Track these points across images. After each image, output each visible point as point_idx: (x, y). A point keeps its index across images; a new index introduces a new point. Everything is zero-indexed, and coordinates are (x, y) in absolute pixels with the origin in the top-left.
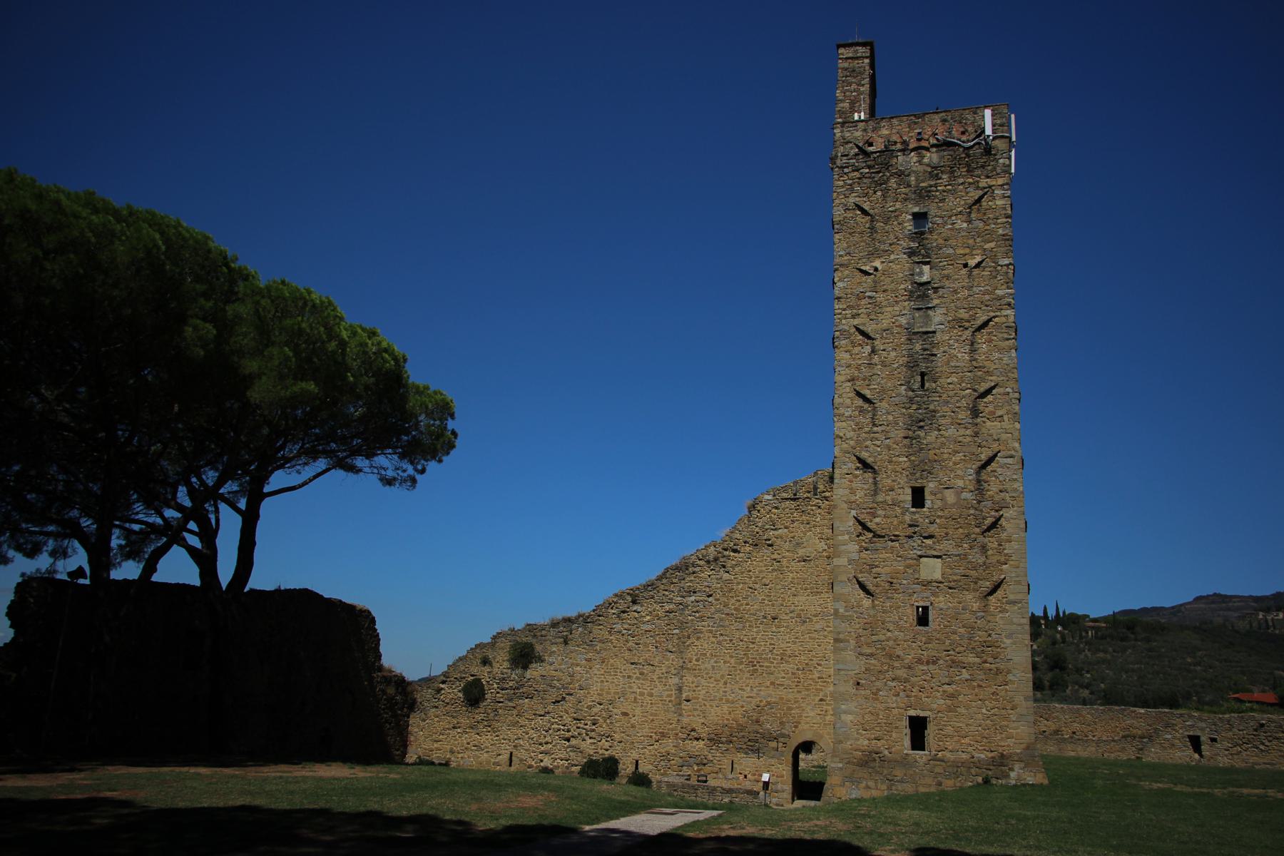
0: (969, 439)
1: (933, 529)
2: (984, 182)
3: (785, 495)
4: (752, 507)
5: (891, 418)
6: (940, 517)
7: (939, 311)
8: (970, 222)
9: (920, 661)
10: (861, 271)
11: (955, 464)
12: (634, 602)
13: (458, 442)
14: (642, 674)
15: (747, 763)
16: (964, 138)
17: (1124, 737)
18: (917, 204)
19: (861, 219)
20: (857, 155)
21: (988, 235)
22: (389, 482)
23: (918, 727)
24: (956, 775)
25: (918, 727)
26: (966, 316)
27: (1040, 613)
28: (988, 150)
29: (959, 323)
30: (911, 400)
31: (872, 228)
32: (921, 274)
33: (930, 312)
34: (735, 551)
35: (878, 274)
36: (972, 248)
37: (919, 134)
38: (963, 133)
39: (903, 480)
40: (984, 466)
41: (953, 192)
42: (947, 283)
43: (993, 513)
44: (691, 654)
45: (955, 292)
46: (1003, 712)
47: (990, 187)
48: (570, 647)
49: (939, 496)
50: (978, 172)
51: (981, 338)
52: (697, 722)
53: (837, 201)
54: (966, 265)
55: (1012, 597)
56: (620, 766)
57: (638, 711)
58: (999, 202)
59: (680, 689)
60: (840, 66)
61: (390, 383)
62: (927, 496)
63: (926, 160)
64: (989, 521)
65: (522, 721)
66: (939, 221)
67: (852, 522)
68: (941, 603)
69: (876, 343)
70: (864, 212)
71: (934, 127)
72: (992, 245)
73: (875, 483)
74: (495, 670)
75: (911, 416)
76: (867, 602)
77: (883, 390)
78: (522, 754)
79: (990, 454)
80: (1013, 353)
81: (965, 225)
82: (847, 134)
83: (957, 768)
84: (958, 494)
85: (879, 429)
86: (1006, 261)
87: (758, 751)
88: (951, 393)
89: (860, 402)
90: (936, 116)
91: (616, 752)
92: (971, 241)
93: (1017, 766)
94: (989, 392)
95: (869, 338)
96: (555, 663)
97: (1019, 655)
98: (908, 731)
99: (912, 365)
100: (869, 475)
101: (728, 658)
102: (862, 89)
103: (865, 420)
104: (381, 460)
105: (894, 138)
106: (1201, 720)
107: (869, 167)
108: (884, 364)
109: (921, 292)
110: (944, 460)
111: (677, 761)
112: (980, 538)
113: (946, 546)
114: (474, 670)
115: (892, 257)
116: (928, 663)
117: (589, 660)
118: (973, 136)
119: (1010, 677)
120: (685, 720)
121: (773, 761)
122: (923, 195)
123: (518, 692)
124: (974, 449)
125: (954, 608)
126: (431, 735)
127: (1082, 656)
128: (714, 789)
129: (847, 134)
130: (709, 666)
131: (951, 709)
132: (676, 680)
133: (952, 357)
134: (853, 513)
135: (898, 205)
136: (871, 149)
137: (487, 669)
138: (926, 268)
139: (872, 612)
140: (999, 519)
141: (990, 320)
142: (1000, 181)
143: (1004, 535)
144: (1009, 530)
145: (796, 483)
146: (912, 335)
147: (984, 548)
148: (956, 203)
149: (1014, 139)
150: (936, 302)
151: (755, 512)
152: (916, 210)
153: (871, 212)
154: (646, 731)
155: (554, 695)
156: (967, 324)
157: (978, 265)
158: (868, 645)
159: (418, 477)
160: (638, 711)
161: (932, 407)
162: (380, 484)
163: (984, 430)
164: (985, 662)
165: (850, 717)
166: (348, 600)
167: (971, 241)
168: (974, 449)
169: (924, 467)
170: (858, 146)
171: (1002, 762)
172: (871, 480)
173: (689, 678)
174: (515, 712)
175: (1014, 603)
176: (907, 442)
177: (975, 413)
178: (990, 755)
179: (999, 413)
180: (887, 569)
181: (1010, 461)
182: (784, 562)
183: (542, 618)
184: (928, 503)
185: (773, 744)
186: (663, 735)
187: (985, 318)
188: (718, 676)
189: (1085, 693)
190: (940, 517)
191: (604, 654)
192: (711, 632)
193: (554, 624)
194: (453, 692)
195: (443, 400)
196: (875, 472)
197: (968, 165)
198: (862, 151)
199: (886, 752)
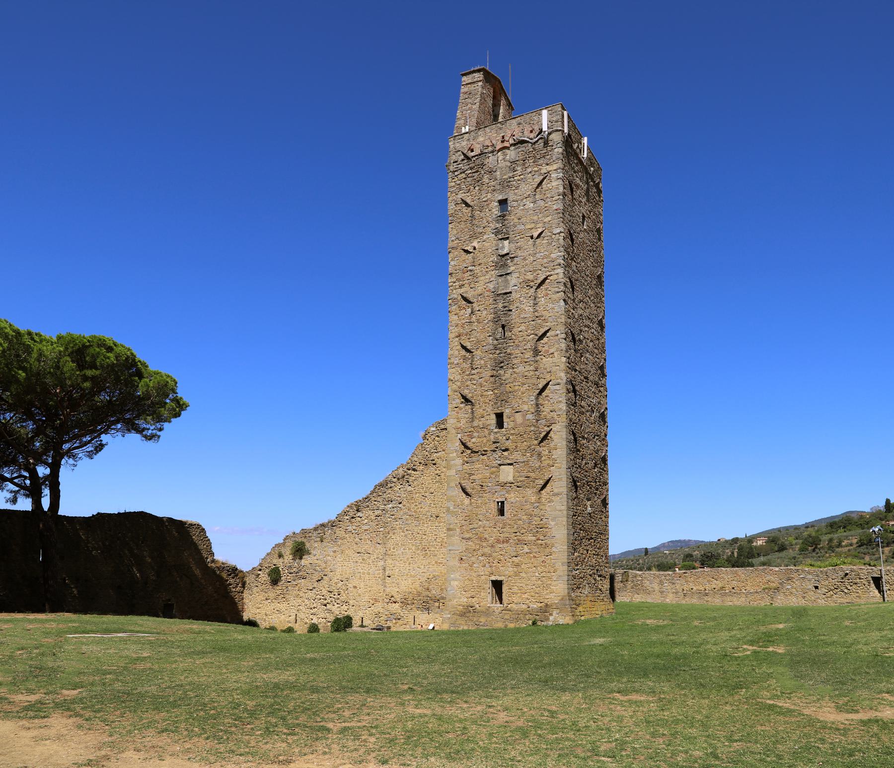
0: (532, 373)
1: (508, 444)
4: (424, 438)
5: (482, 362)
6: (512, 434)
7: (515, 275)
8: (534, 202)
9: (498, 541)
12: (358, 511)
16: (532, 135)
17: (764, 589)
18: (501, 192)
20: (463, 160)
23: (497, 586)
25: (497, 586)
29: (527, 284)
30: (496, 348)
32: (503, 247)
33: (509, 277)
34: (414, 470)
38: (531, 132)
39: (489, 409)
40: (540, 393)
42: (519, 253)
44: (390, 544)
45: (525, 259)
48: (324, 544)
49: (512, 419)
50: (541, 161)
52: (393, 590)
54: (532, 237)
55: (556, 491)
56: (353, 622)
58: (554, 184)
59: (384, 569)
61: (130, 368)
62: (505, 419)
65: (301, 594)
66: (515, 204)
67: (458, 442)
68: (512, 498)
70: (467, 205)
73: (473, 413)
74: (286, 561)
75: (495, 360)
76: (467, 501)
77: (478, 342)
78: (301, 615)
79: (545, 383)
80: (562, 303)
81: (532, 205)
83: (518, 615)
84: (524, 416)
86: (558, 231)
87: (428, 609)
89: (463, 352)
92: (535, 218)
95: (470, 302)
99: (496, 320)
101: (411, 546)
102: (474, 107)
103: (466, 366)
105: (488, 143)
106: (809, 573)
107: (471, 169)
108: (478, 321)
110: (515, 391)
112: (538, 448)
113: (516, 456)
114: (275, 561)
115: (485, 237)
116: (503, 542)
117: (335, 552)
119: (554, 549)
120: (388, 590)
122: (506, 184)
123: (299, 575)
126: (256, 604)
129: (458, 145)
131: (517, 574)
132: (381, 563)
135: (489, 196)
137: (281, 560)
138: (506, 243)
139: (470, 508)
140: (548, 433)
141: (546, 279)
142: (555, 167)
143: (552, 445)
144: (556, 440)
147: (539, 455)
148: (526, 188)
150: (512, 268)
152: (500, 198)
154: (366, 598)
156: (532, 284)
160: (362, 585)
161: (509, 351)
163: (541, 365)
164: (538, 539)
165: (456, 583)
166: (682, 538)
167: (535, 218)
169: (502, 399)
171: (546, 609)
172: (470, 411)
174: (297, 588)
175: (557, 494)
176: (492, 379)
177: (536, 352)
178: (540, 605)
179: (551, 351)
180: (480, 476)
181: (557, 387)
183: (310, 526)
185: (437, 604)
186: (376, 600)
188: (405, 559)
190: (512, 434)
191: (343, 547)
192: (401, 528)
193: (316, 529)
194: (264, 577)
198: (467, 157)
199: (477, 606)
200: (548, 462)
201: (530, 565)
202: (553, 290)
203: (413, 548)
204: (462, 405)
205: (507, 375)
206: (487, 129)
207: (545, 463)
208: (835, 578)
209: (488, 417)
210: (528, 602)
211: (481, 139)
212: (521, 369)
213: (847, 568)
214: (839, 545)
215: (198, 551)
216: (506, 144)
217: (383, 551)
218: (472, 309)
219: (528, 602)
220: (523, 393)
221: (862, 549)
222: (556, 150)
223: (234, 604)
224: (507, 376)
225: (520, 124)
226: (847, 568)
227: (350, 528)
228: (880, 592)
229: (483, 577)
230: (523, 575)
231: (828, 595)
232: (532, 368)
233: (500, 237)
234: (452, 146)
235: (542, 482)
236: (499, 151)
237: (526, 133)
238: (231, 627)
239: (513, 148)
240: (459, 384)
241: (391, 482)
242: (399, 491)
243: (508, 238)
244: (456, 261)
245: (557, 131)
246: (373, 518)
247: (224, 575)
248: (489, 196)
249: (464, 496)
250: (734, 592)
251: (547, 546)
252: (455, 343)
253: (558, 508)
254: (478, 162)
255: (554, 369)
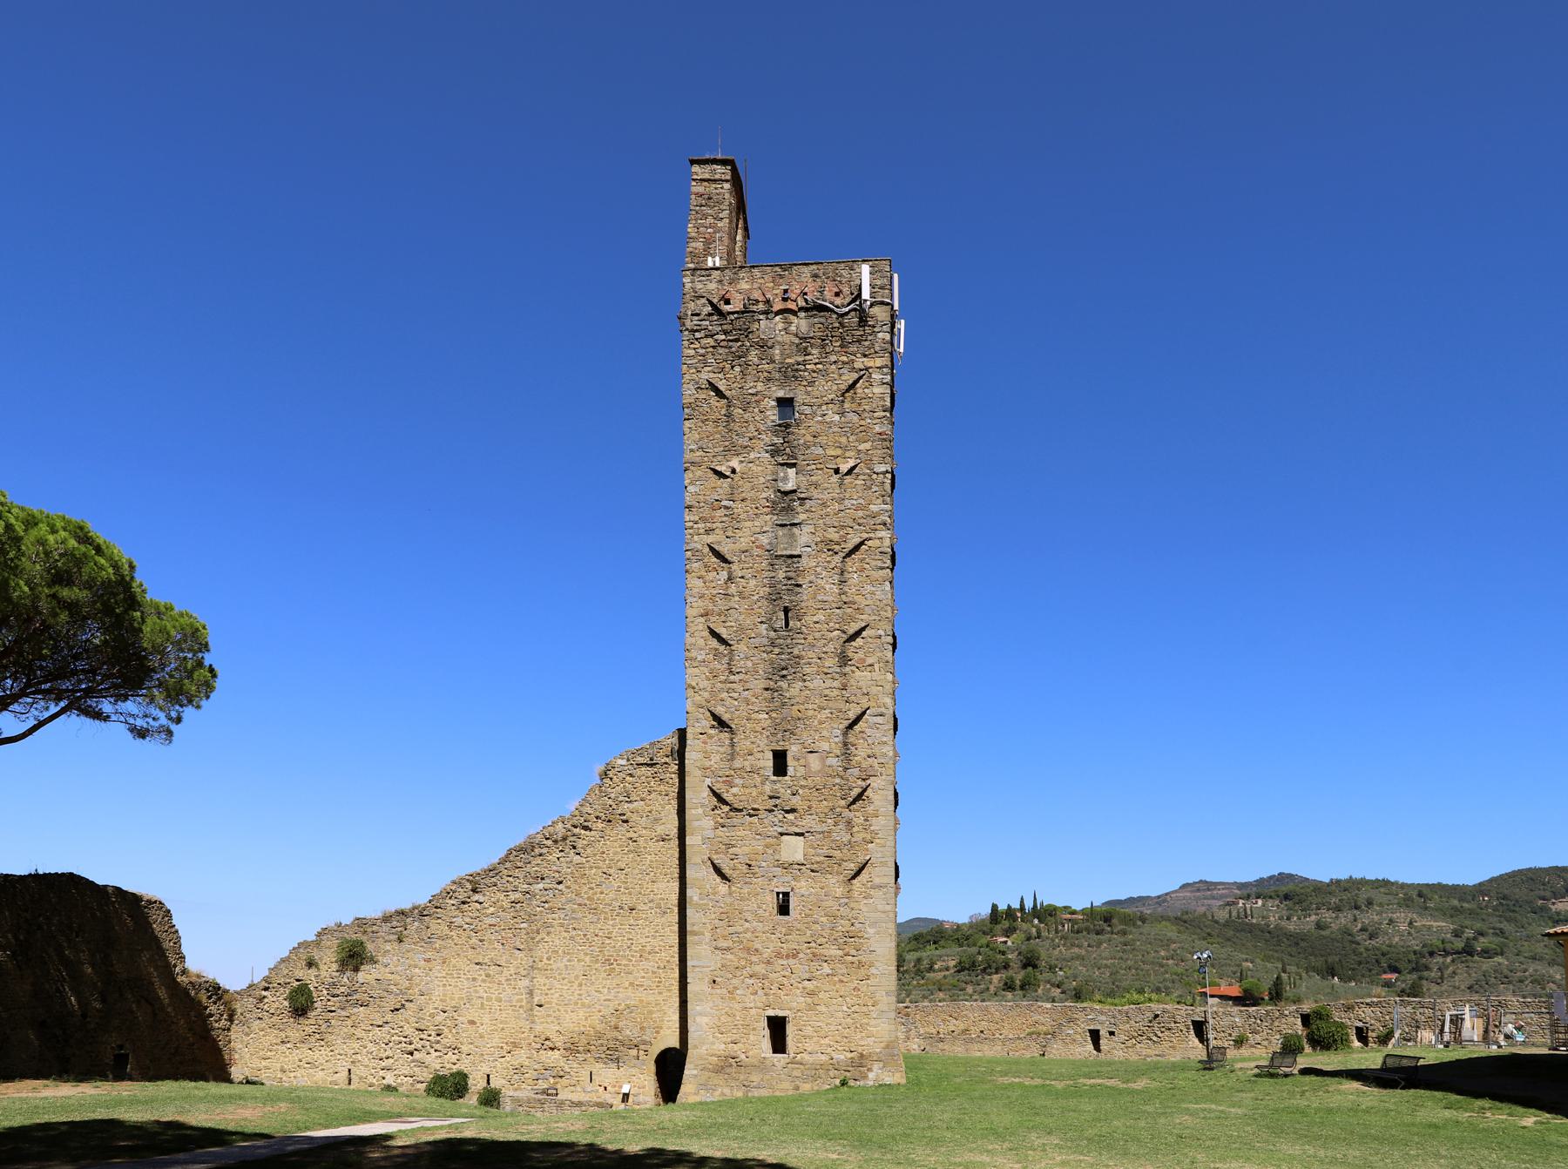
0: (836, 692)
1: (796, 802)
2: (860, 363)
3: (640, 760)
4: (605, 774)
5: (749, 664)
7: (807, 529)
8: (842, 414)
9: (779, 955)
10: (716, 472)
11: (821, 723)
12: (474, 891)
13: (218, 683)
14: (488, 976)
15: (607, 1074)
16: (838, 301)
18: (781, 386)
19: (714, 401)
20: (710, 314)
21: (862, 432)
22: (141, 733)
23: (777, 1027)
24: (815, 1078)
25: (777, 1027)
26: (835, 537)
27: (1016, 905)
28: (863, 319)
29: (829, 546)
30: (773, 644)
31: (728, 415)
32: (785, 479)
33: (795, 530)
34: (586, 828)
35: (736, 477)
36: (845, 449)
37: (786, 291)
38: (837, 294)
39: (762, 742)
40: (851, 726)
41: (825, 373)
42: (815, 493)
43: (859, 782)
44: (541, 951)
45: (824, 505)
46: (865, 1009)
47: (867, 369)
48: (405, 946)
49: (802, 762)
50: (853, 348)
51: (852, 564)
52: (551, 1030)
53: (687, 377)
54: (837, 471)
55: (877, 881)
56: (470, 1082)
57: (486, 1019)
58: (877, 390)
59: (531, 993)
60: (694, 189)
61: (118, 598)
63: (793, 328)
64: (856, 792)
65: (359, 1033)
66: (808, 410)
67: (707, 792)
68: (802, 890)
69: (734, 567)
71: (803, 283)
72: (867, 446)
73: (732, 745)
74: (323, 974)
75: (772, 663)
76: (723, 888)
80: (887, 586)
81: (837, 417)
82: (699, 286)
83: (816, 1071)
84: (823, 760)
85: (736, 678)
86: (882, 468)
88: (817, 635)
89: (714, 643)
90: (805, 269)
91: (463, 1066)
92: (844, 440)
93: (876, 1067)
94: (858, 633)
95: (725, 561)
96: (390, 965)
97: (882, 950)
98: (767, 1032)
99: (774, 597)
100: (725, 736)
101: (582, 956)
102: (720, 224)
103: (720, 666)
104: (130, 706)
105: (756, 295)
106: (1102, 1013)
107: (725, 333)
109: (786, 500)
110: (808, 718)
111: (532, 1074)
112: (846, 813)
114: (300, 974)
115: (752, 456)
116: (788, 957)
117: (428, 960)
118: (848, 300)
119: (873, 970)
120: (538, 1028)
121: (634, 1071)
122: (790, 374)
123: (353, 999)
124: (842, 705)
125: (816, 894)
126: (254, 1049)
127: (1056, 952)
128: (562, 1102)
129: (699, 286)
130: (561, 965)
133: (820, 589)
134: (708, 781)
136: (727, 308)
137: (313, 972)
138: (791, 472)
139: (729, 900)
141: (862, 543)
143: (870, 809)
145: (653, 744)
146: (775, 558)
148: (827, 388)
149: (896, 307)
150: (802, 517)
151: (607, 781)
152: (781, 394)
153: (727, 393)
154: (496, 1041)
155: (392, 1002)
156: (837, 548)
157: (850, 472)
158: (725, 938)
159: (173, 727)
160: (486, 1019)
161: (796, 652)
162: (129, 735)
165: (705, 1020)
167: (844, 440)
168: (842, 705)
170: (711, 303)
171: (861, 1062)
172: (727, 742)
173: (540, 980)
174: (349, 1022)
175: (880, 887)
176: (767, 694)
177: (844, 660)
178: (849, 1055)
179: (869, 661)
180: (747, 850)
182: (641, 841)
183: (373, 911)
184: (790, 771)
185: (634, 1052)
186: (515, 1045)
187: (857, 540)
189: (1056, 992)
191: (445, 953)
193: (386, 919)
194: (278, 1001)
195: (191, 625)
196: (732, 731)
197: (843, 339)
198: (717, 310)
200: (862, 835)
201: (833, 994)
202: (874, 563)
203: (587, 959)
204: (712, 732)
205: (794, 690)
206: (755, 271)
207: (859, 837)
208: (1140, 1021)
209: (759, 755)
210: (829, 1050)
211: (744, 286)
212: (817, 683)
213: (1157, 1008)
214: (931, 969)
215: (161, 952)
216: (792, 306)
217: (527, 962)
218: (730, 574)
219: (829, 1050)
220: (821, 723)
221: (964, 976)
222: (880, 335)
223: (218, 1052)
224: (794, 691)
225: (816, 276)
226: (1157, 1008)
227: (458, 921)
228: (1202, 1041)
229: (753, 1012)
230: (822, 1008)
231: (1129, 1044)
232: (836, 684)
233: (780, 460)
234: (688, 286)
235: (853, 867)
236: (777, 313)
237: (828, 295)
238: (224, 1085)
239: (802, 314)
240: (706, 695)
241: (540, 845)
242: (556, 861)
243: (794, 465)
244: (697, 486)
245: (882, 303)
246: (506, 904)
247: (203, 996)
248: (760, 386)
249: (718, 879)
250: (982, 1036)
251: (861, 964)
252: (699, 626)
253: (880, 907)
254: (738, 324)
255: (874, 690)
